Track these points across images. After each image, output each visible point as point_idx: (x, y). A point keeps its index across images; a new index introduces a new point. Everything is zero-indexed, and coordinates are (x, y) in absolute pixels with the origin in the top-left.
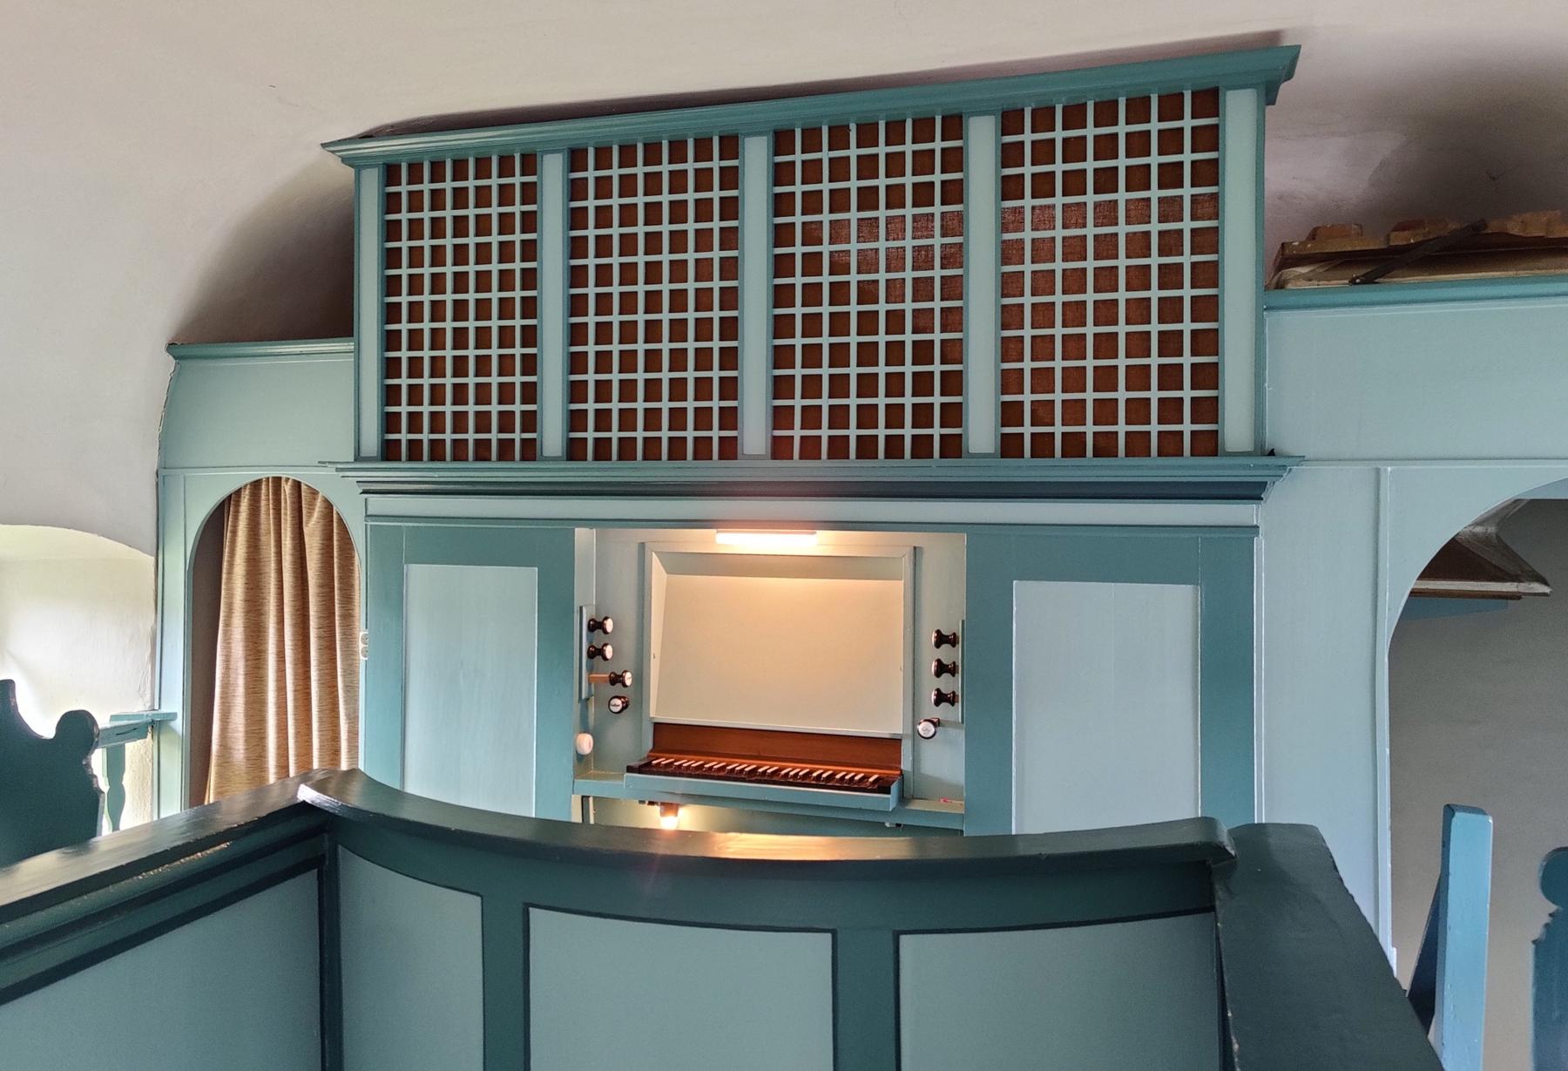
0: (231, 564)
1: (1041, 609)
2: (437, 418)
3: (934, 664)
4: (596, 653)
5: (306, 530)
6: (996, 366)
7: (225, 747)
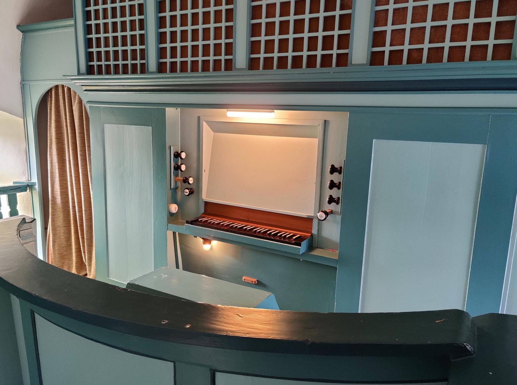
0: (51, 123)
1: (387, 155)
2: (184, 49)
3: (329, 182)
4: (177, 168)
5: (73, 108)
6: (372, 9)
7: (54, 197)
